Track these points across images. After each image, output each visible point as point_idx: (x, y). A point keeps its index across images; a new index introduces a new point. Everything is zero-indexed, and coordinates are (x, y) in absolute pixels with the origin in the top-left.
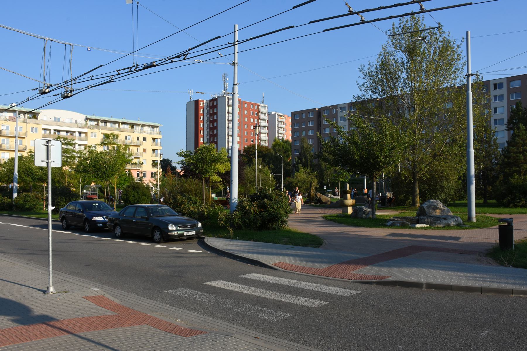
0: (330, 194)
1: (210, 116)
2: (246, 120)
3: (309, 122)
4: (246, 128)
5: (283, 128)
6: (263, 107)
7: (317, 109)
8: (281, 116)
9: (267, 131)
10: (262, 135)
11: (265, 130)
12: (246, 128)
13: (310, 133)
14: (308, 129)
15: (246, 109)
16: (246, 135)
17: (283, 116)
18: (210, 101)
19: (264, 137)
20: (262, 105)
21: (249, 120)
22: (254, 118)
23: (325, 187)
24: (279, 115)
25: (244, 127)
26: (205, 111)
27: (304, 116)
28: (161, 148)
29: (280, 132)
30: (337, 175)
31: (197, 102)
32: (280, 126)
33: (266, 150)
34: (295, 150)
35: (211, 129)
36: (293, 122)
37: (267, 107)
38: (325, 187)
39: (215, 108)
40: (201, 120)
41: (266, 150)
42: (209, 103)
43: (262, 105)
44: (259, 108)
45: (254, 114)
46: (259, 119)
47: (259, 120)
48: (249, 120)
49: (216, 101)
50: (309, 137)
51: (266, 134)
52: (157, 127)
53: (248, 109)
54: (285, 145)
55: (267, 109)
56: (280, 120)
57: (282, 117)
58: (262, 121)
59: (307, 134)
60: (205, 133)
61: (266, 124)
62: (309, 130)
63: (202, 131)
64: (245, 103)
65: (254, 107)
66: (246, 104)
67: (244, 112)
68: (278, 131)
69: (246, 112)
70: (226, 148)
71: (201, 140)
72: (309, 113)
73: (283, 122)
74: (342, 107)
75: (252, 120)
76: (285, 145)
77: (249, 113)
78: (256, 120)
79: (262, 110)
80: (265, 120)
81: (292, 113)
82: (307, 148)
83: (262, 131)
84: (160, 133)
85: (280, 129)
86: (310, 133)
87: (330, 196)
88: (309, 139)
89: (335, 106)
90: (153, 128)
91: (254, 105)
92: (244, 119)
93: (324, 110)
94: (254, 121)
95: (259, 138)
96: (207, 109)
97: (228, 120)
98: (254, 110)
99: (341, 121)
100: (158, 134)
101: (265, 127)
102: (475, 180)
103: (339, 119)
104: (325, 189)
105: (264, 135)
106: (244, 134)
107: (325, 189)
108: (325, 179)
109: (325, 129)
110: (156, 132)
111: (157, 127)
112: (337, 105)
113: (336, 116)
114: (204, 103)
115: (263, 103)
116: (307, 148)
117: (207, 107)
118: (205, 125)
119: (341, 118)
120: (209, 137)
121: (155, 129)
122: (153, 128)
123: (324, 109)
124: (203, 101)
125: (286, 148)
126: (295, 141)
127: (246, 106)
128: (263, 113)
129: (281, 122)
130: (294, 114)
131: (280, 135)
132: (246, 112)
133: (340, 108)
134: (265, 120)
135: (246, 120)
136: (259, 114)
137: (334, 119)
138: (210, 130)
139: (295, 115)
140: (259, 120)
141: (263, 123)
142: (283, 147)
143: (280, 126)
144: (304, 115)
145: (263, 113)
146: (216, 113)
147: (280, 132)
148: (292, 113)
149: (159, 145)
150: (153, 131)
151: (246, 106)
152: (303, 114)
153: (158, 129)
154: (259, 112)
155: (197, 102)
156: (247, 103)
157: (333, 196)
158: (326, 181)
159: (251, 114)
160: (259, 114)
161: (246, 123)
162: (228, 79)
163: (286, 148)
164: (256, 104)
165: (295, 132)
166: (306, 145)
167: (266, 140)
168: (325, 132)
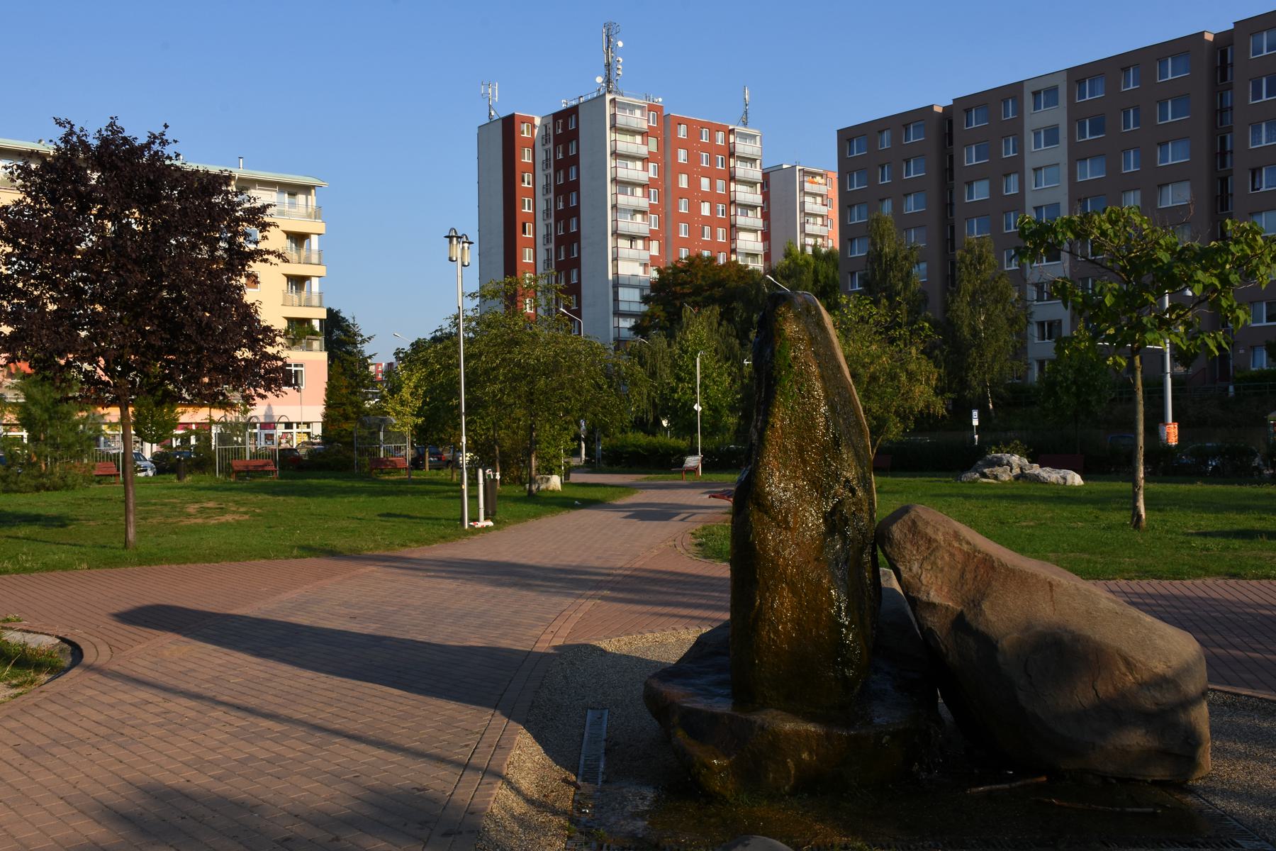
0: (1015, 459)
1: (556, 171)
2: (683, 182)
3: (908, 162)
4: (683, 210)
5: (822, 216)
6: (745, 136)
7: (938, 109)
8: (814, 175)
9: (759, 223)
10: (742, 236)
11: (755, 220)
12: (683, 210)
13: (911, 206)
14: (902, 191)
15: (683, 144)
16: (683, 235)
17: (821, 175)
18: (557, 116)
19: (749, 242)
20: (740, 129)
21: (694, 183)
22: (712, 175)
23: (975, 413)
24: (805, 173)
25: (677, 207)
26: (541, 156)
27: (886, 141)
28: (321, 271)
29: (809, 228)
30: (1120, 296)
31: (509, 123)
32: (808, 208)
33: (739, 278)
34: (853, 274)
35: (559, 216)
36: (846, 169)
37: (758, 138)
38: (975, 413)
39: (571, 141)
40: (526, 185)
41: (739, 278)
42: (551, 126)
43: (740, 129)
44: (731, 141)
45: (712, 161)
46: (732, 178)
47: (732, 185)
48: (694, 183)
49: (573, 117)
50: (907, 224)
51: (755, 231)
52: (306, 189)
53: (691, 144)
54: (823, 267)
55: (758, 144)
56: (808, 187)
57: (818, 179)
58: (740, 188)
59: (897, 208)
60: (542, 230)
61: (757, 198)
62: (906, 195)
63: (529, 226)
64: (680, 122)
65: (712, 137)
66: (683, 129)
67: (676, 156)
68: (803, 225)
69: (682, 155)
70: (610, 277)
71: (527, 257)
72: (906, 127)
73: (821, 196)
74: (1044, 92)
75: (705, 183)
76: (823, 267)
77: (693, 159)
78: (720, 184)
79: (742, 147)
80: (752, 184)
81: (841, 133)
82: (895, 258)
83: (741, 221)
84: (317, 214)
85: (811, 220)
86: (911, 206)
87: (1017, 471)
88: (908, 229)
89: (1012, 92)
90: (292, 194)
91: (714, 129)
92: (676, 181)
93: (968, 111)
94: (713, 185)
95: (733, 246)
96: (546, 147)
97: (615, 180)
98: (711, 148)
99: (1037, 145)
100: (309, 216)
101: (753, 207)
102: (1144, 405)
103: (1029, 139)
104: (975, 422)
105: (751, 236)
106: (677, 230)
107: (975, 422)
108: (974, 383)
109: (970, 184)
110: (303, 210)
111: (306, 189)
112: (1019, 86)
113: (1015, 130)
114: (534, 126)
115: (745, 124)
116: (895, 258)
117: (546, 139)
118: (541, 206)
119: (1037, 133)
120: (552, 246)
121: (301, 198)
122: (292, 194)
123: (965, 105)
124: (530, 121)
125: (827, 277)
126: (852, 240)
127: (682, 132)
128: (745, 159)
129: (814, 195)
130: (846, 137)
131: (810, 241)
132: (682, 155)
133: (1036, 94)
134: (752, 184)
135: (683, 182)
136: (732, 161)
137: (1007, 142)
138: (556, 221)
139: (850, 141)
140: (732, 185)
141: (744, 194)
142: (816, 272)
143: (808, 208)
144: (886, 135)
145: (745, 159)
146: (575, 160)
147: (809, 228)
148: (841, 133)
149: (315, 259)
150: (292, 205)
151: (682, 132)
152: (881, 132)
153: (312, 199)
154: (732, 154)
155: (509, 123)
156: (688, 122)
157: (1036, 469)
158: (979, 390)
159: (700, 161)
160: (732, 161)
161: (682, 194)
162: (620, 44)
163: (827, 277)
164: (719, 128)
165: (851, 207)
166: (893, 245)
167: (757, 255)
168: (971, 196)
